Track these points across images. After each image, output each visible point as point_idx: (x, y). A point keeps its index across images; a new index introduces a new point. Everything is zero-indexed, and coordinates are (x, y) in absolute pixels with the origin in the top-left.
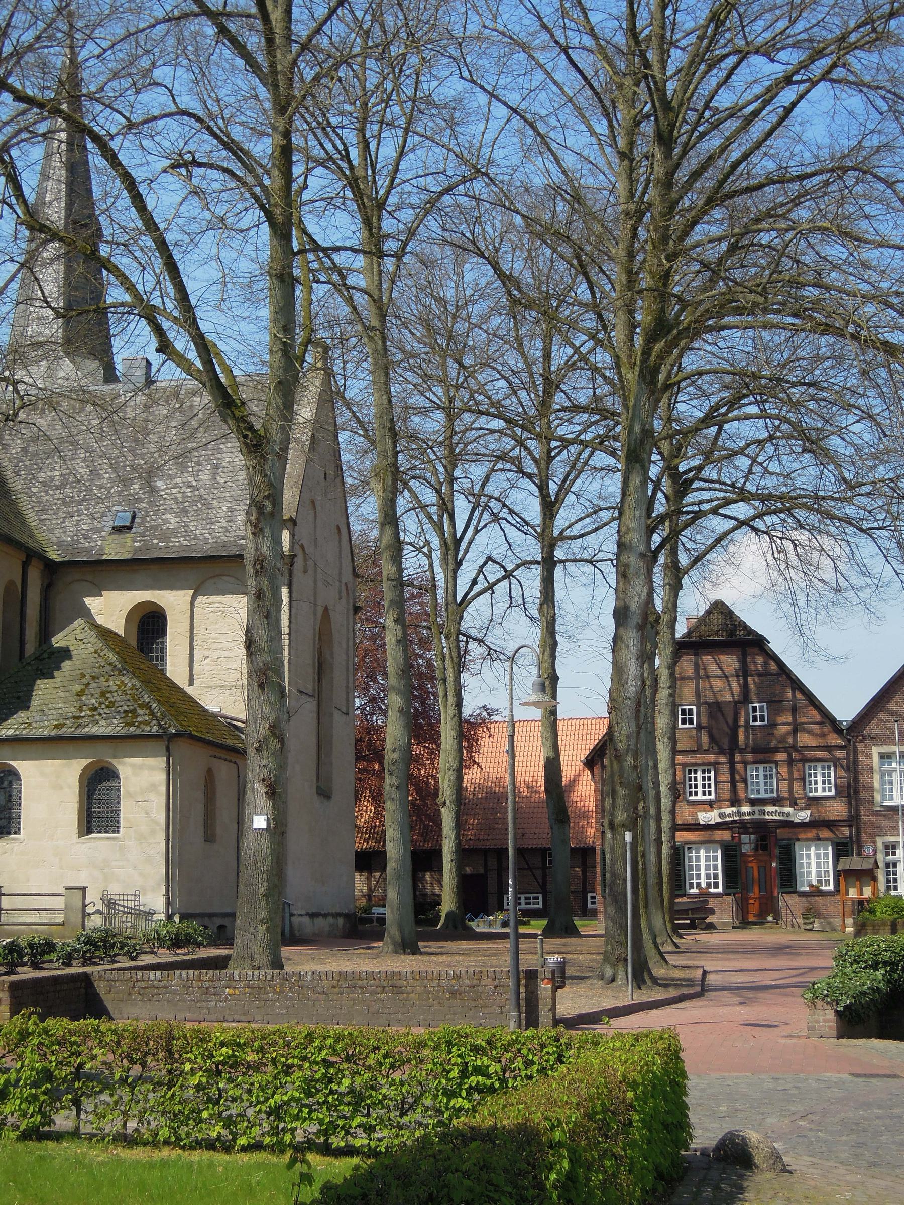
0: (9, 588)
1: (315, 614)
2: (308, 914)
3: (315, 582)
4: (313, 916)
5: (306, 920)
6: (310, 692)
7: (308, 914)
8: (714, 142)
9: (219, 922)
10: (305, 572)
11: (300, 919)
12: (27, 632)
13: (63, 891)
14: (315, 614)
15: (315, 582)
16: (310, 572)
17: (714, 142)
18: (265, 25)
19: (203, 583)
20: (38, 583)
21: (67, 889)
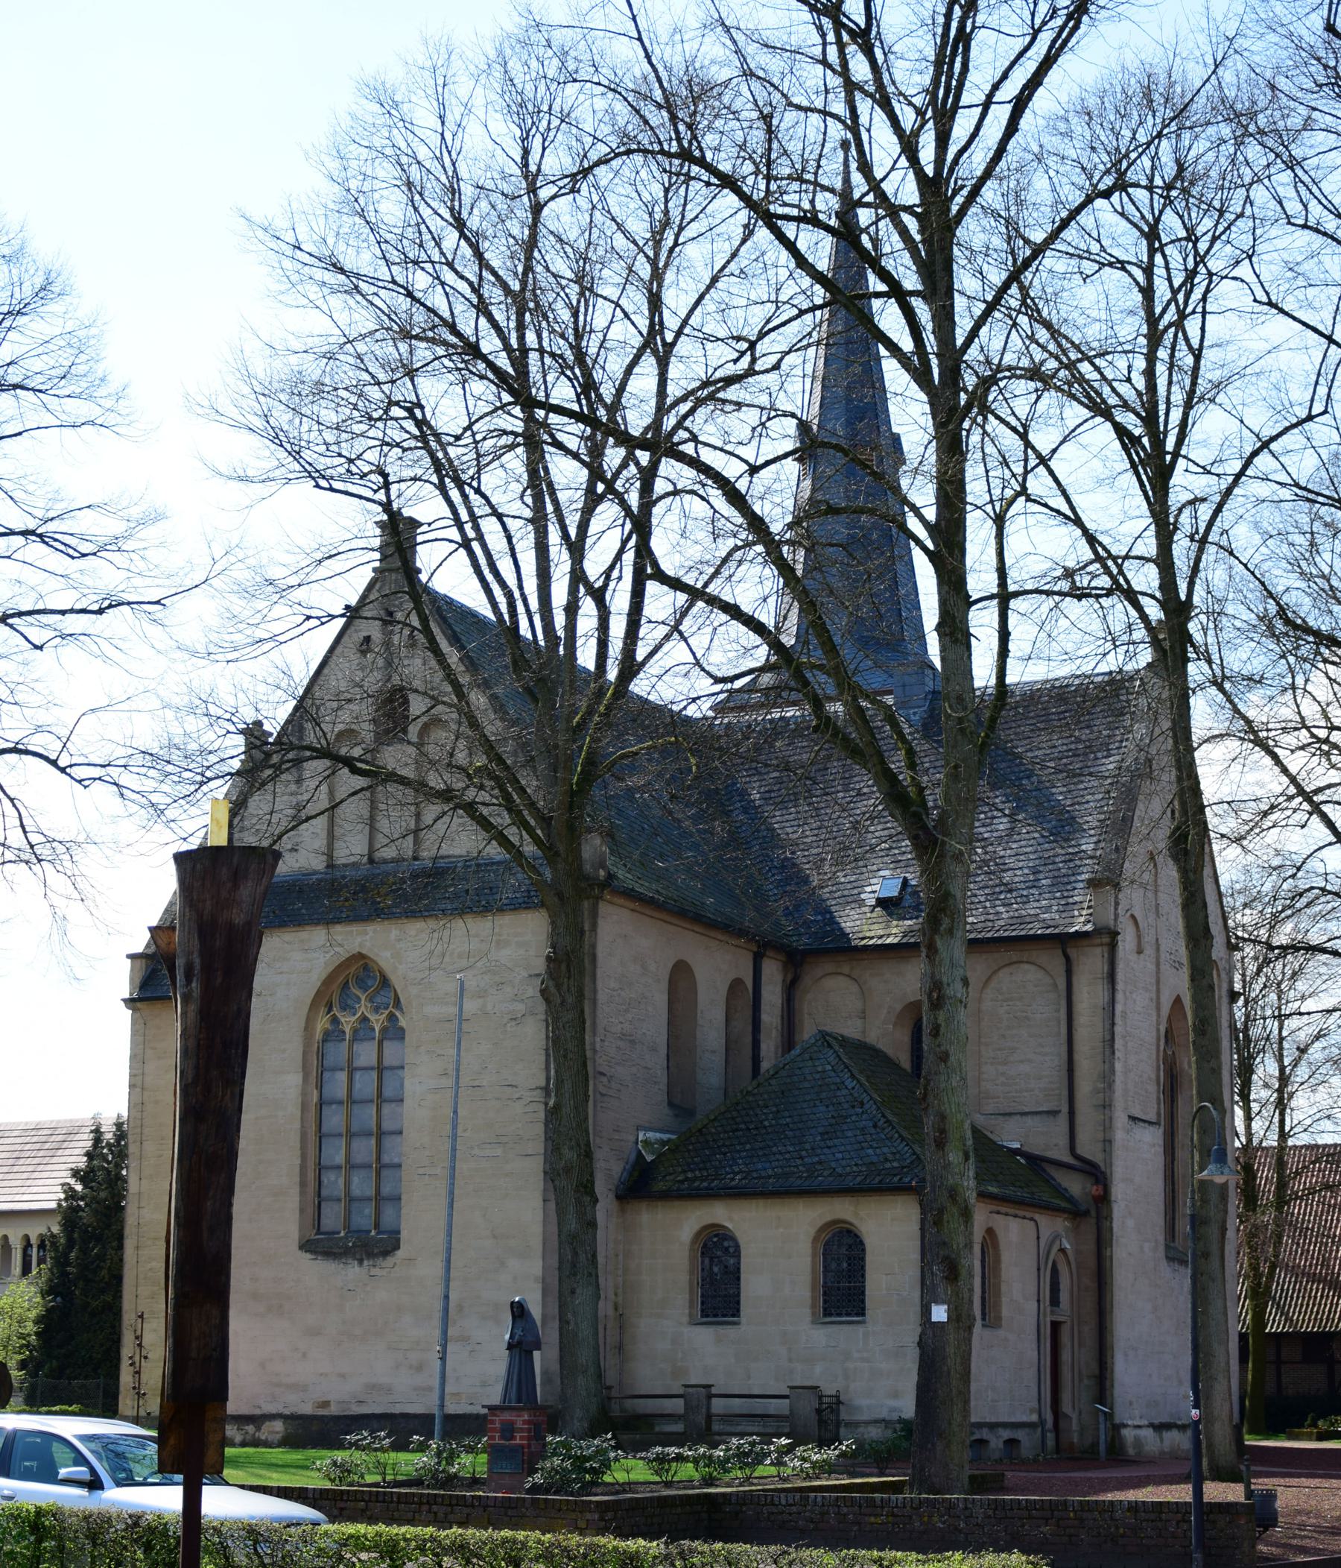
0: (736, 985)
1: (1158, 1009)
2: (1152, 1425)
3: (1158, 965)
4: (1160, 1428)
5: (1148, 1434)
6: (1152, 1117)
7: (1152, 1425)
8: (882, 833)
9: (1006, 1434)
10: (1140, 952)
11: (1138, 1432)
12: (763, 1046)
13: (787, 1392)
14: (1158, 1009)
15: (1158, 965)
16: (1149, 951)
17: (882, 833)
18: (883, 268)
19: (995, 972)
20: (778, 978)
21: (791, 1388)
